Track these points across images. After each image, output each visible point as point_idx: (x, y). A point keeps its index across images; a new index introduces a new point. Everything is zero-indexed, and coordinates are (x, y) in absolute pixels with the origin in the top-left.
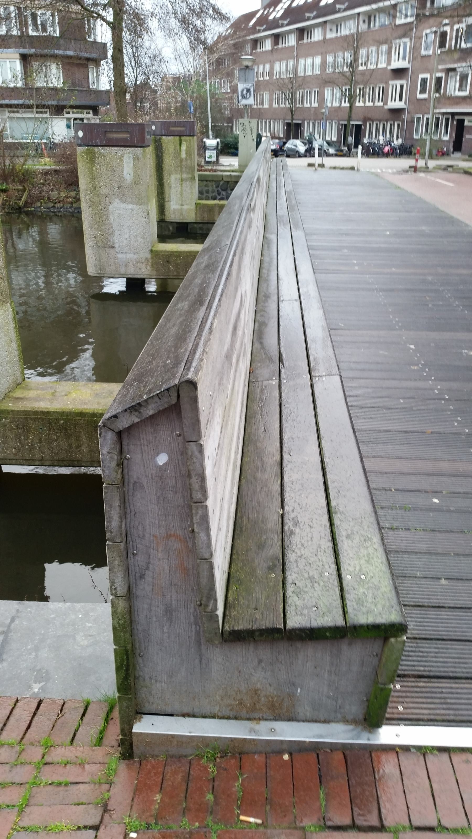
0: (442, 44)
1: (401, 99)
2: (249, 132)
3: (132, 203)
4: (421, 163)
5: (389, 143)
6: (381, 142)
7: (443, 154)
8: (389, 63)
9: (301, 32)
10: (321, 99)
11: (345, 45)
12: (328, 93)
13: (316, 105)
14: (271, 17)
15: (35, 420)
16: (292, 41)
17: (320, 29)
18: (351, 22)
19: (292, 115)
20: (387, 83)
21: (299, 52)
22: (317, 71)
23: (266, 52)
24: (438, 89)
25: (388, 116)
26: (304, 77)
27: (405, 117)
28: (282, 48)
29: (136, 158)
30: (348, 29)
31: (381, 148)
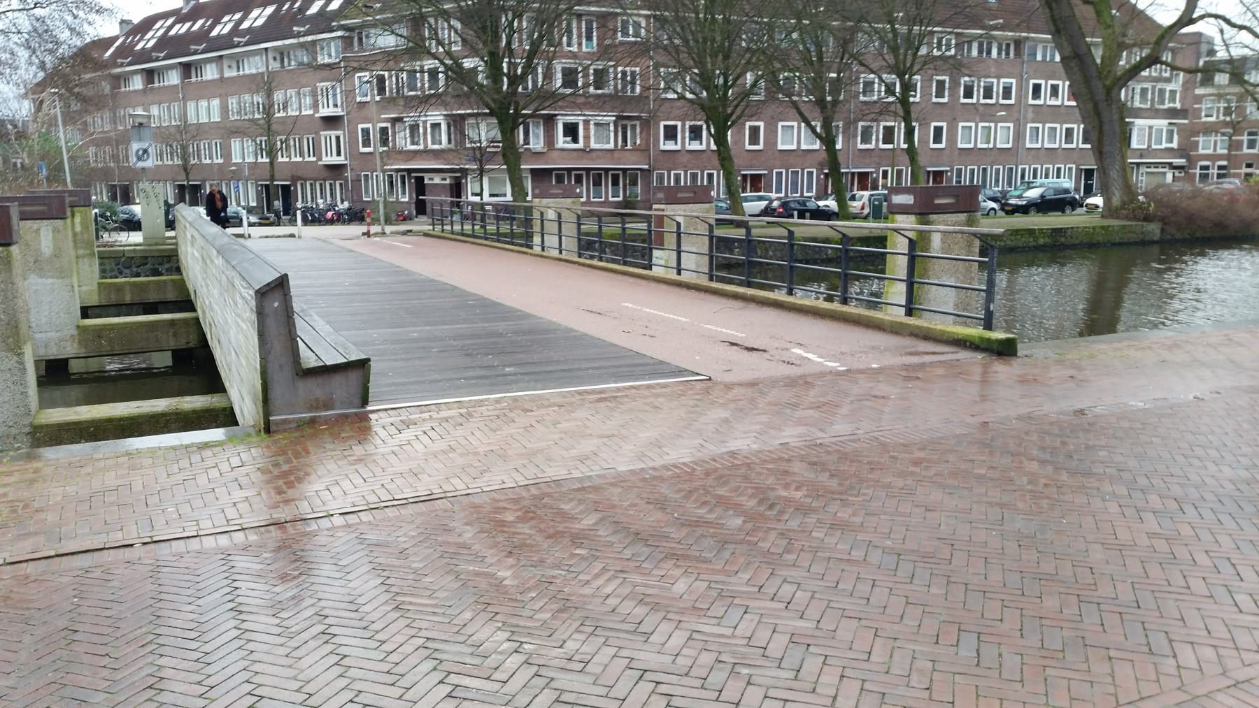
0: (382, 90)
1: (339, 154)
2: (153, 199)
3: (52, 277)
4: (375, 229)
5: (332, 207)
6: (321, 206)
7: (406, 219)
8: (315, 106)
9: (187, 69)
10: (227, 154)
11: (254, 87)
12: (235, 145)
13: (220, 161)
14: (139, 47)
15: (67, 431)
16: (174, 78)
17: (214, 65)
18: (258, 58)
19: (187, 175)
20: (317, 133)
21: (187, 92)
22: (216, 118)
23: (135, 91)
24: (384, 142)
25: (326, 174)
26: (199, 125)
27: (348, 174)
28: (159, 88)
29: (56, 231)
30: (253, 67)
31: (323, 213)
